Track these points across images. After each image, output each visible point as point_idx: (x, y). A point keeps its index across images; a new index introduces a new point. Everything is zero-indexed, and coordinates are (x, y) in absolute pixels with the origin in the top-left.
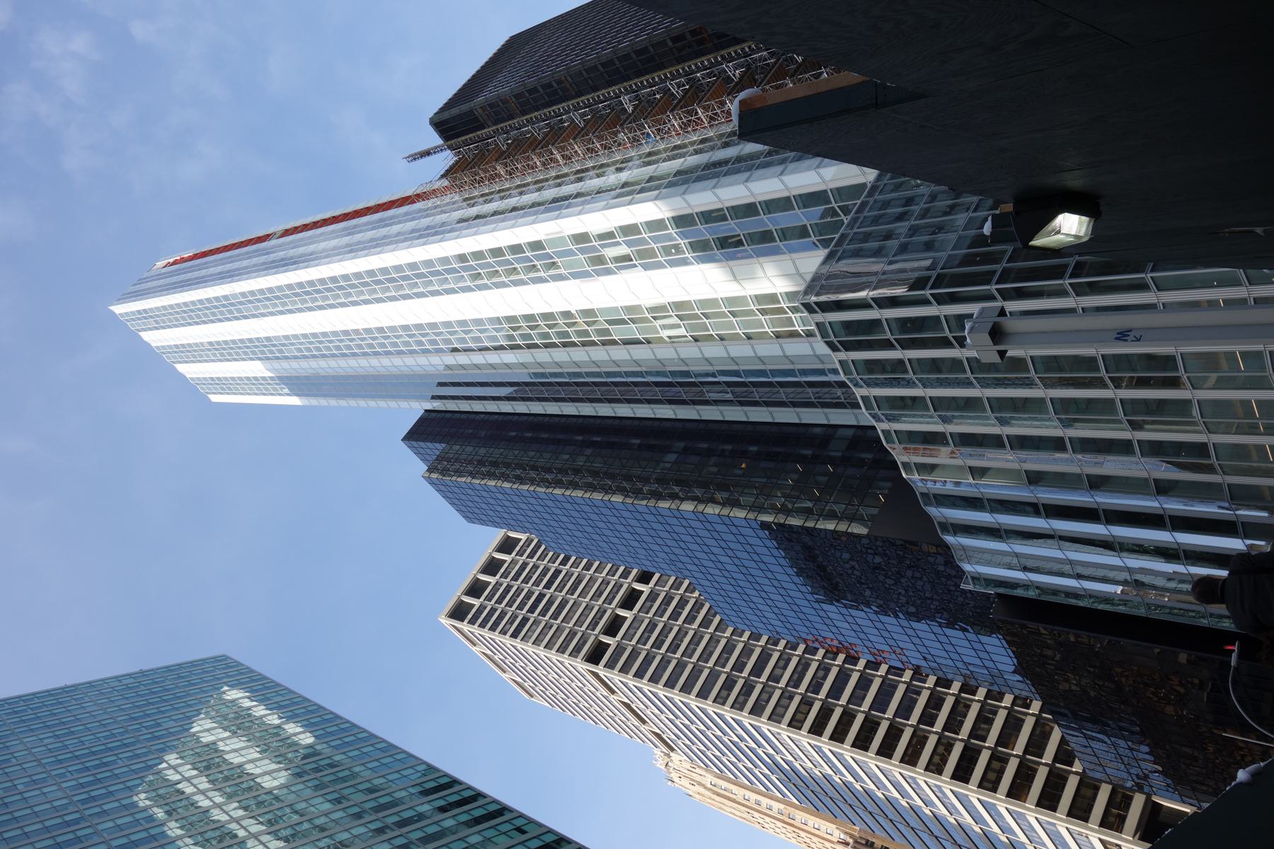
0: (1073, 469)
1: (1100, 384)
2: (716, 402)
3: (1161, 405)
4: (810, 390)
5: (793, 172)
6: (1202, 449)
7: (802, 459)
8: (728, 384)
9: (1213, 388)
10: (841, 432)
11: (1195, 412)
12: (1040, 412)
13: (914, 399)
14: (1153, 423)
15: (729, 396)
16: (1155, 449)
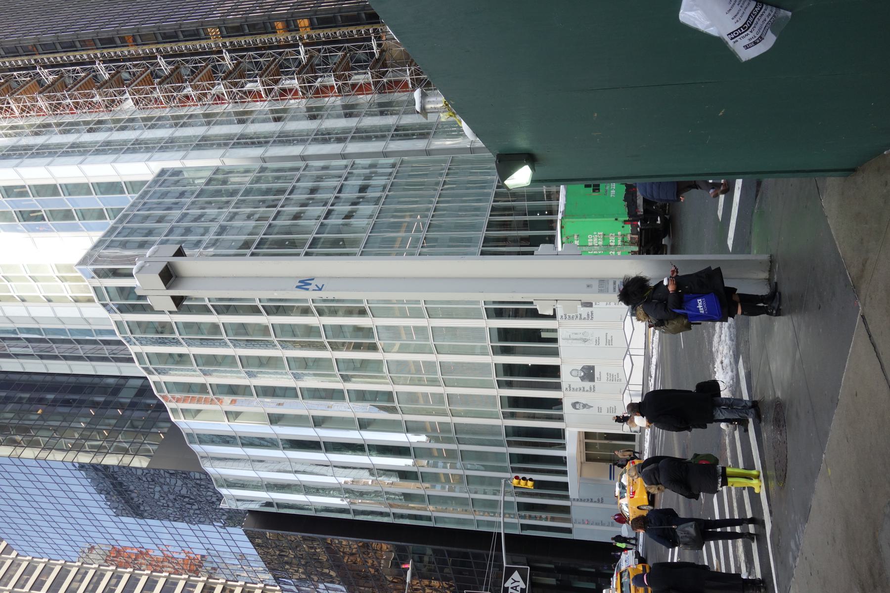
0: (304, 412)
1: (321, 347)
2: (17, 356)
3: (364, 363)
4: (105, 347)
5: (92, 163)
6: (389, 396)
7: (94, 405)
8: (29, 340)
9: (398, 352)
10: (131, 382)
11: (385, 369)
12: (276, 368)
13: (225, 357)
14: (359, 376)
15: (30, 351)
16: (361, 396)
